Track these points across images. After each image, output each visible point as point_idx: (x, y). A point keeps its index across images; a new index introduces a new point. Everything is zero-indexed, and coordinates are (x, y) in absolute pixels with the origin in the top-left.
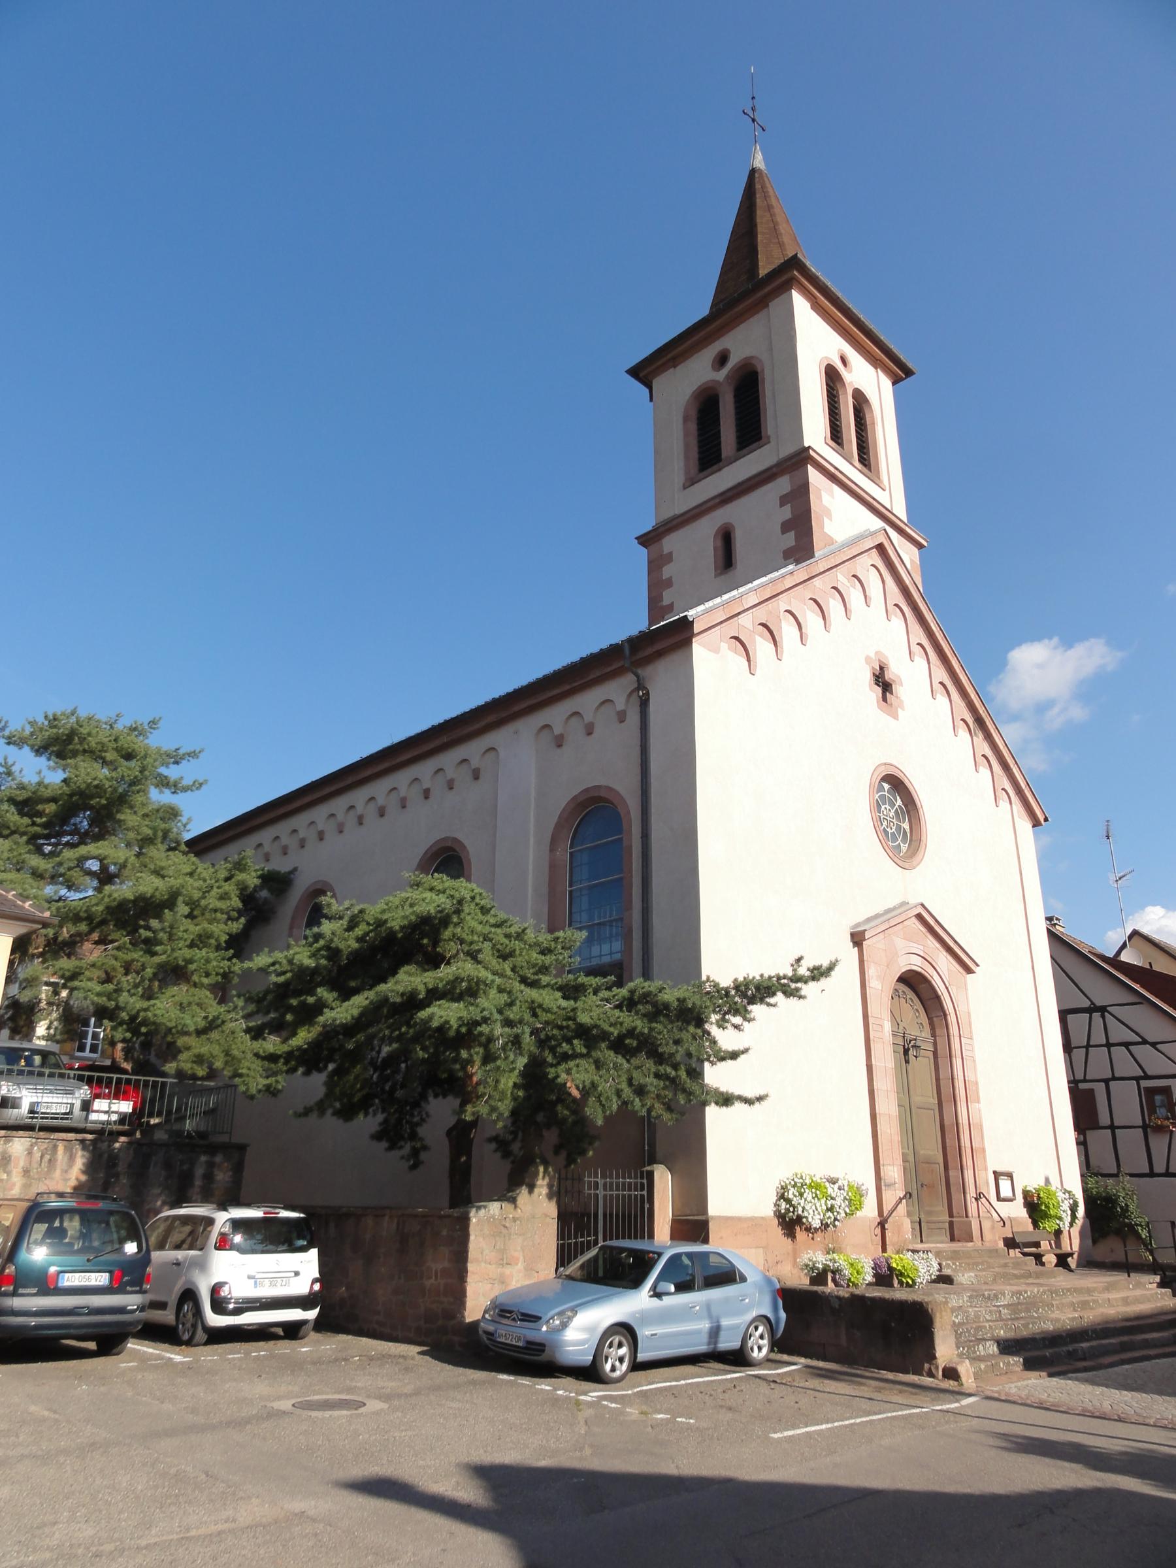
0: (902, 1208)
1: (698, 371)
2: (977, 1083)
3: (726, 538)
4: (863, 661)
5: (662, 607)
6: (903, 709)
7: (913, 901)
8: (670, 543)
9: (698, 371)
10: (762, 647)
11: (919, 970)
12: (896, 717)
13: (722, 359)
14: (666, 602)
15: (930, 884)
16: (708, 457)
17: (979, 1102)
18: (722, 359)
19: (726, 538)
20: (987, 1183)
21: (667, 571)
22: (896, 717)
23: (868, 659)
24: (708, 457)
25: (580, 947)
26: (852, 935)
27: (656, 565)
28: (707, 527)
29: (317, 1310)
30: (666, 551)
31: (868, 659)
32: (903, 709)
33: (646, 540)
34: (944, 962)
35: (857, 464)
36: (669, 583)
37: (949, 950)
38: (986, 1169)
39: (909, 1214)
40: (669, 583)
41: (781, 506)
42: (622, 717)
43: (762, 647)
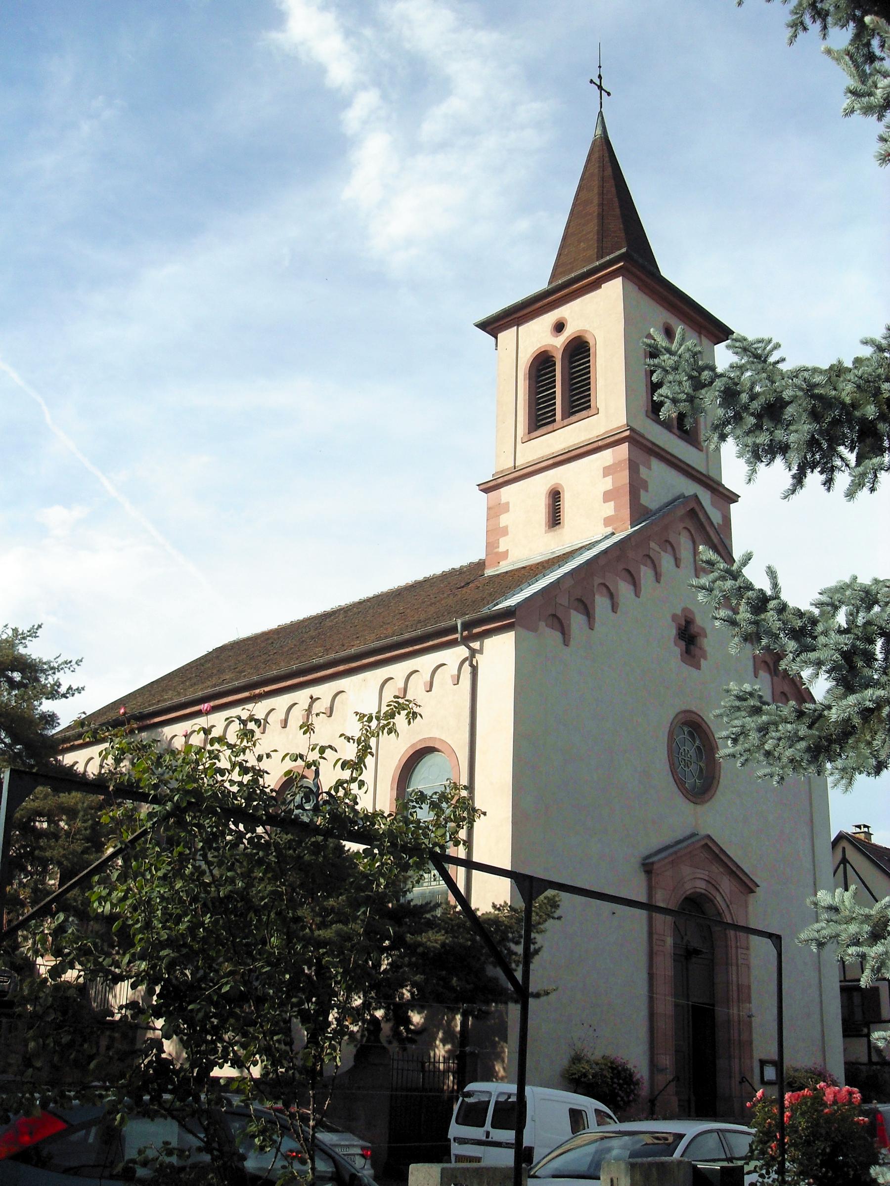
0: (672, 1089)
1: (537, 335)
2: (749, 987)
3: (555, 496)
4: (670, 620)
5: (497, 553)
6: (705, 659)
7: (703, 832)
8: (506, 493)
9: (537, 335)
10: (577, 620)
11: (703, 891)
12: (698, 667)
13: (559, 327)
14: (502, 549)
15: (717, 820)
16: (540, 418)
17: (750, 1002)
18: (559, 327)
19: (555, 496)
20: (752, 1071)
21: (504, 520)
22: (698, 667)
23: (674, 617)
24: (540, 418)
25: (418, 916)
26: (644, 865)
27: (495, 512)
28: (541, 484)
29: (212, 1074)
30: (503, 501)
31: (674, 617)
32: (705, 659)
33: (488, 488)
34: (726, 885)
35: (676, 430)
36: (505, 532)
37: (732, 873)
38: (751, 1057)
39: (677, 1093)
40: (505, 532)
41: (604, 477)
42: (457, 680)
43: (577, 620)
